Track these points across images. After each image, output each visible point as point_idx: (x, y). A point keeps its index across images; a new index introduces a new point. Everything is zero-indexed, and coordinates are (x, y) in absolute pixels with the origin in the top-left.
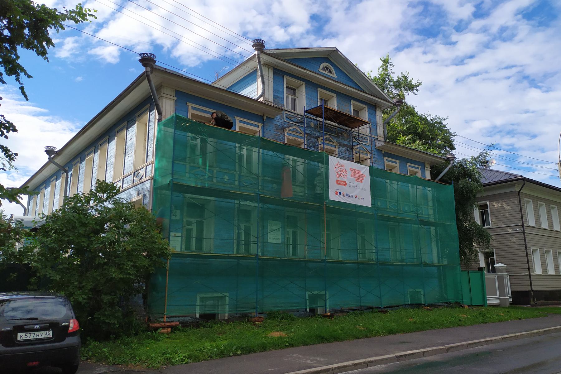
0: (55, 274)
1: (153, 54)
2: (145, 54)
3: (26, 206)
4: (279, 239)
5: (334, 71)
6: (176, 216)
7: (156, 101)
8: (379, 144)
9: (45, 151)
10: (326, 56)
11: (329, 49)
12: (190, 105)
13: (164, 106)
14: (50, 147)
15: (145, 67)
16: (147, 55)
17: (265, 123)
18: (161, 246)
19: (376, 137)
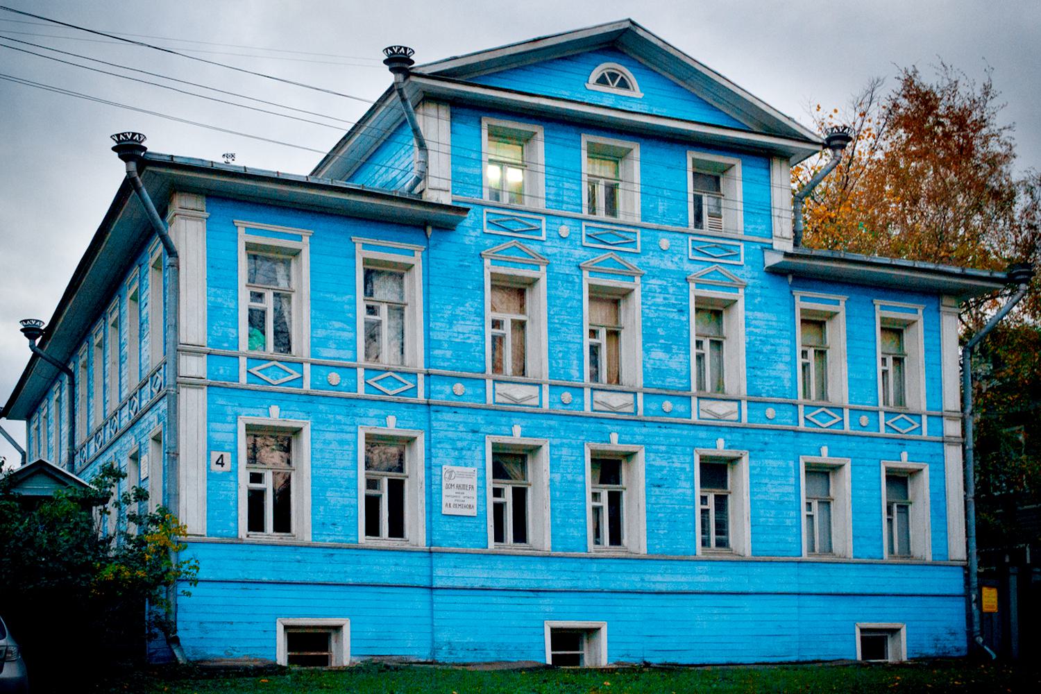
4: (470, 507)
6: (222, 464)
9: (22, 330)
13: (182, 235)
14: (29, 320)
15: (125, 161)
16: (126, 137)
17: (432, 242)
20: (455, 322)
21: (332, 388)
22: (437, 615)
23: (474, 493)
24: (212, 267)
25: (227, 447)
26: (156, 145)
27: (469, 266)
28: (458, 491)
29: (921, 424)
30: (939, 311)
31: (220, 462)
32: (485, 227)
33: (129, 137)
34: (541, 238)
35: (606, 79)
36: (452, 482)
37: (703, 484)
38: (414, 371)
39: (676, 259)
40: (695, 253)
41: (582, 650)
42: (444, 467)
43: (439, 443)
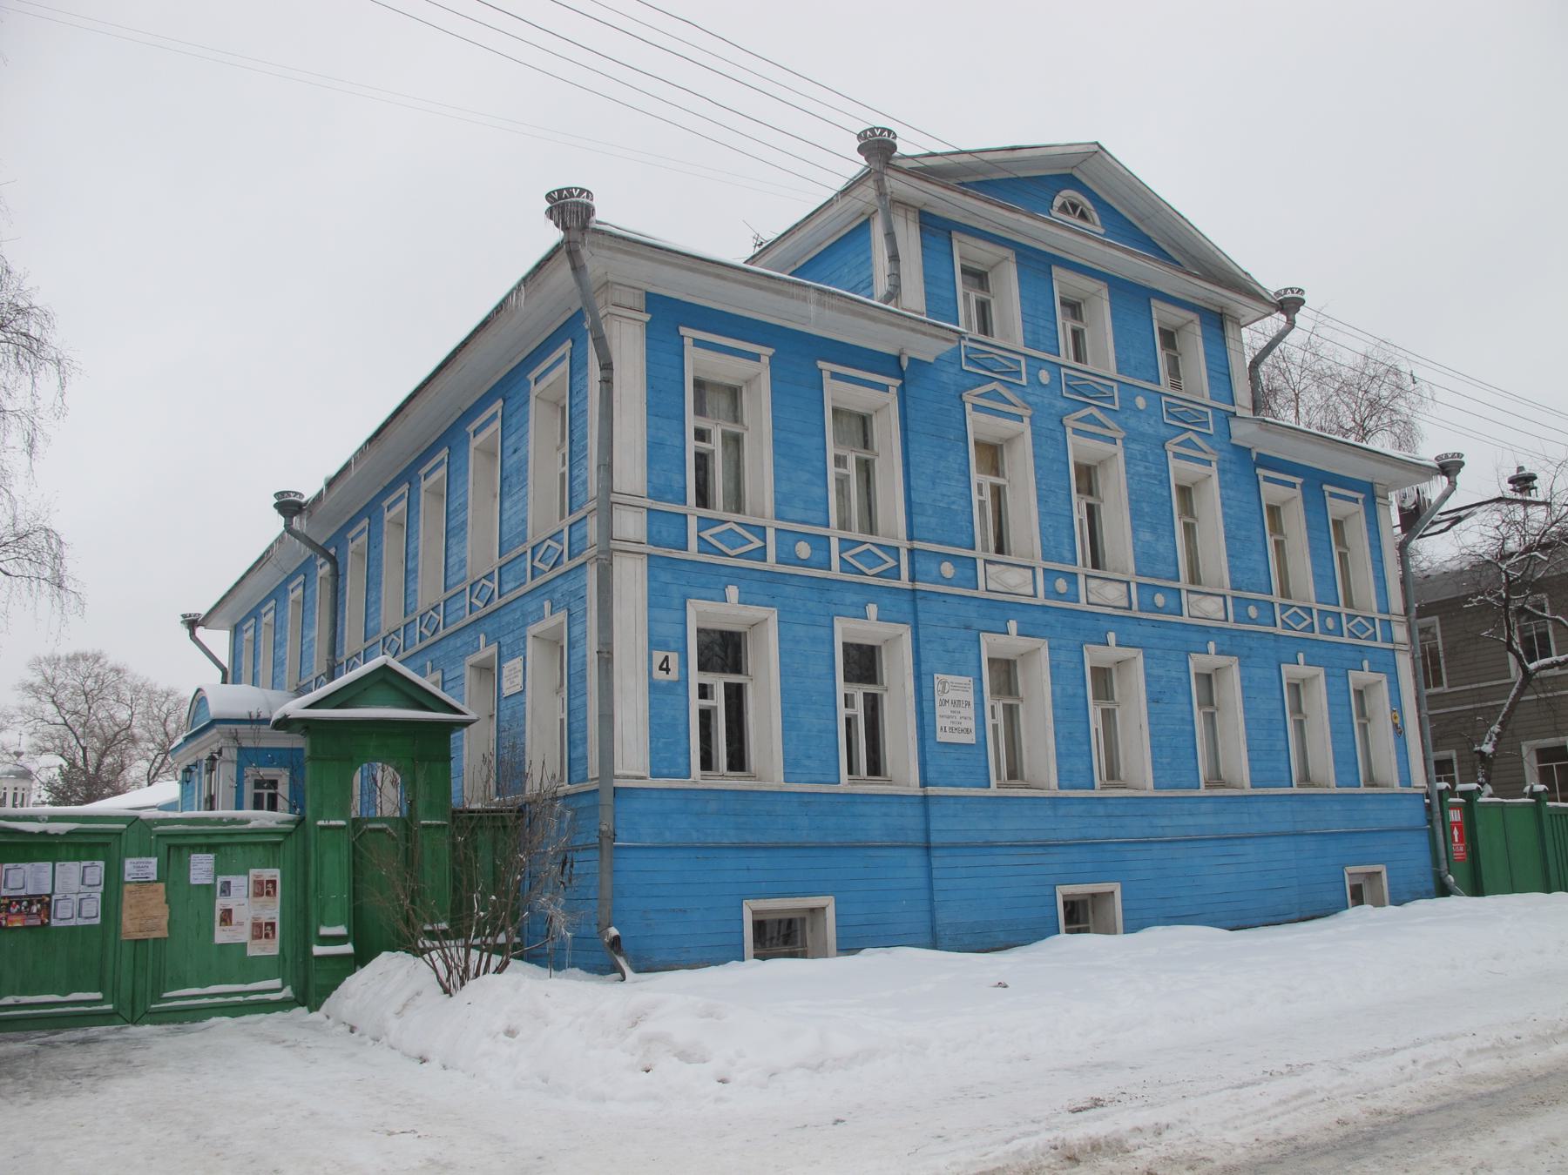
3: (226, 662)
4: (968, 731)
5: (1095, 215)
6: (667, 670)
7: (596, 326)
11: (1076, 148)
18: (21, 1081)
19: (1231, 409)
20: (938, 481)
22: (937, 885)
24: (653, 388)
25: (673, 645)
26: (608, 213)
27: (949, 410)
29: (898, 561)
31: (665, 666)
36: (946, 697)
42: (936, 676)
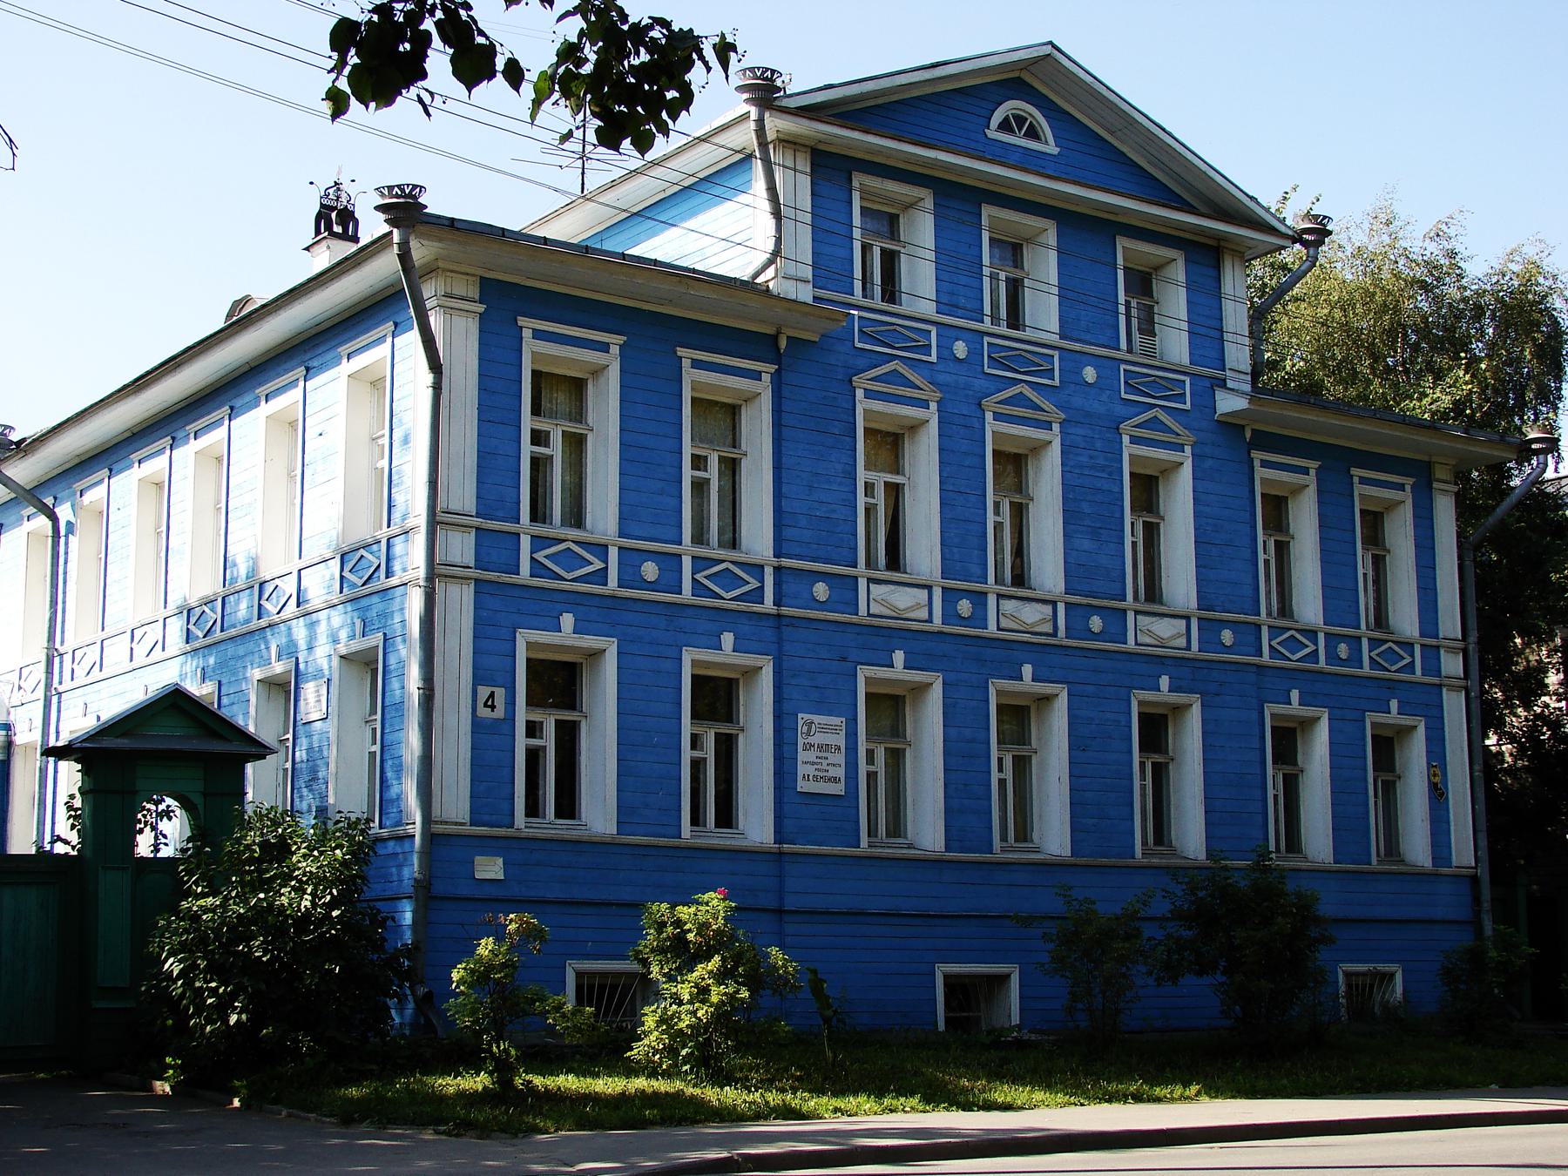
0: (1052, 1096)
1: (418, 186)
2: (396, 189)
4: (835, 780)
6: (493, 707)
8: (1228, 403)
10: (1016, 74)
12: (528, 325)
16: (403, 190)
21: (817, 605)
23: (840, 758)
26: (436, 203)
28: (820, 754)
30: (1431, 488)
31: (490, 703)
32: (1123, 393)
33: (407, 191)
34: (929, 359)
35: (1024, 123)
36: (811, 740)
37: (531, 702)
38: (603, 542)
39: (1104, 398)
40: (1128, 390)
41: (980, 1011)
43: (794, 676)
